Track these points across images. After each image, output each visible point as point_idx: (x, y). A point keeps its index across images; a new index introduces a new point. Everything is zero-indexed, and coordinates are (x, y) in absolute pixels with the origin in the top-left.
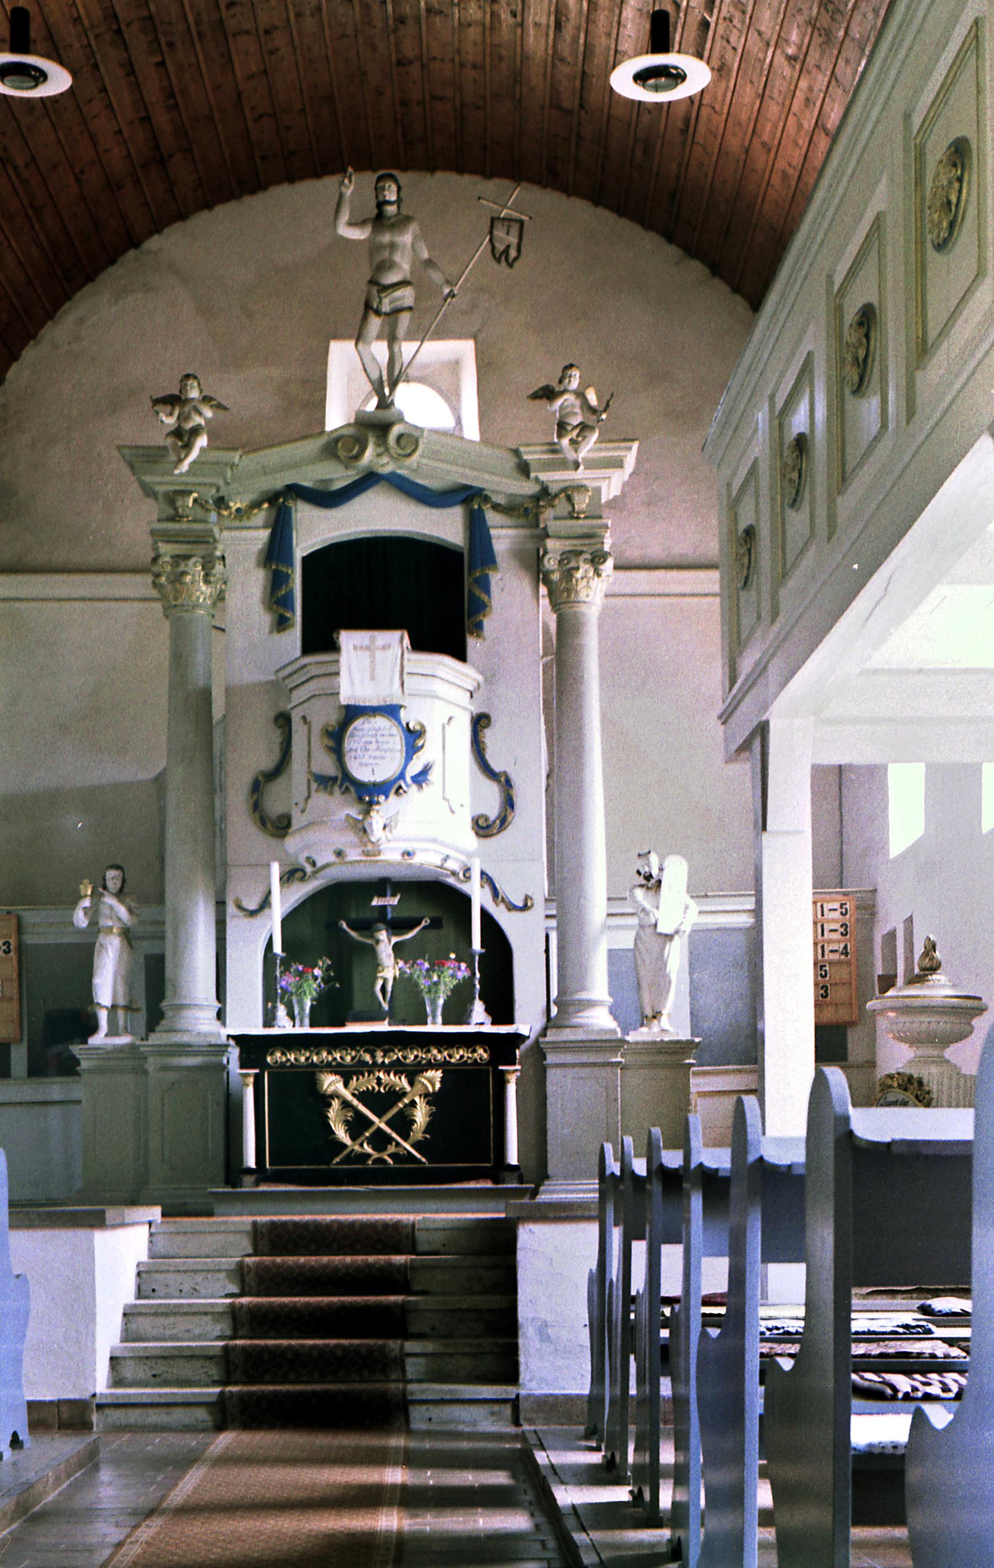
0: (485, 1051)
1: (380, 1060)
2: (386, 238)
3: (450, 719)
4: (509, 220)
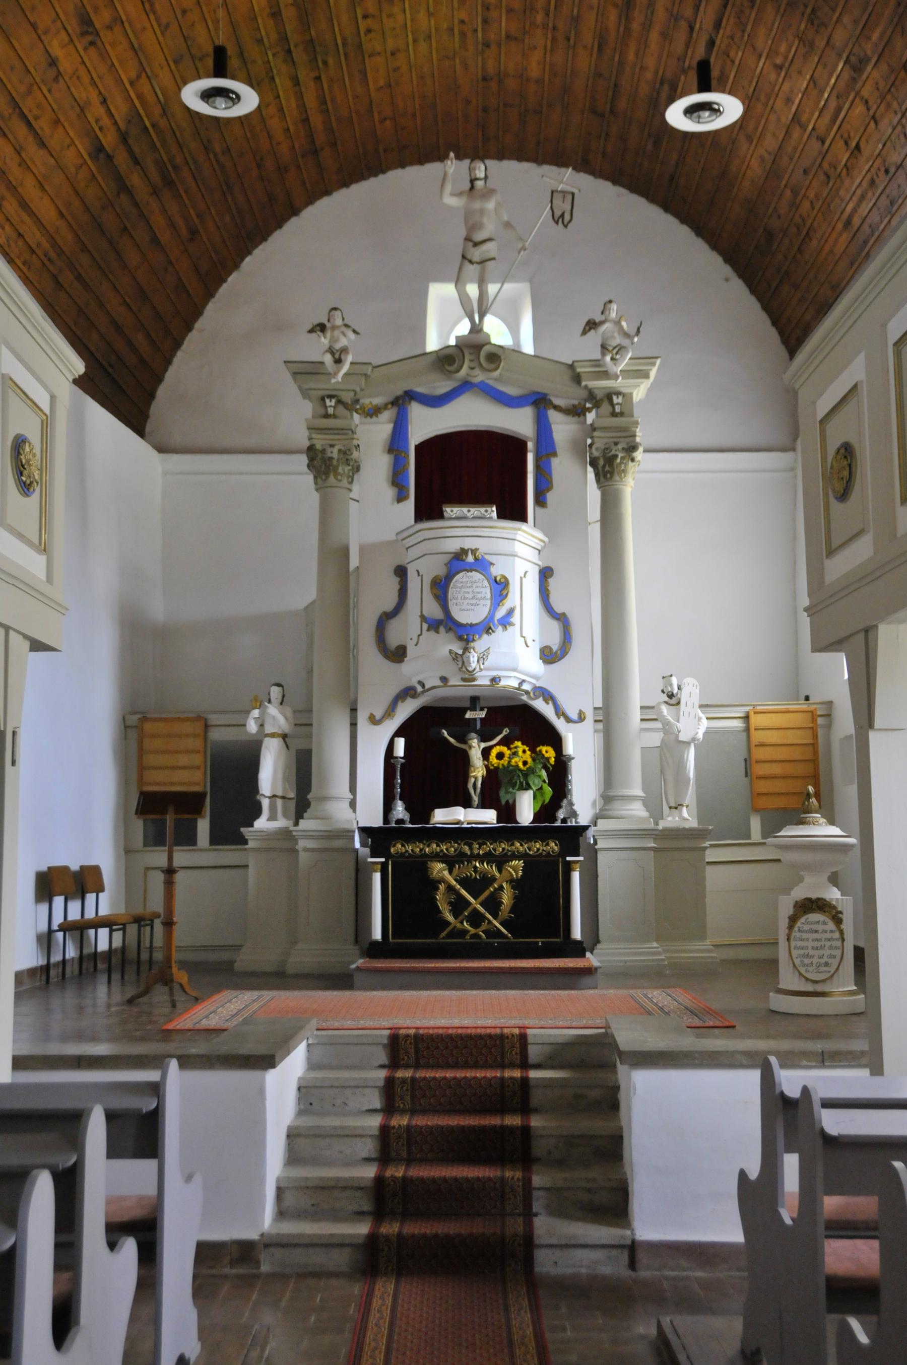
0: (556, 845)
1: (476, 852)
2: (477, 205)
3: (526, 573)
4: (564, 192)
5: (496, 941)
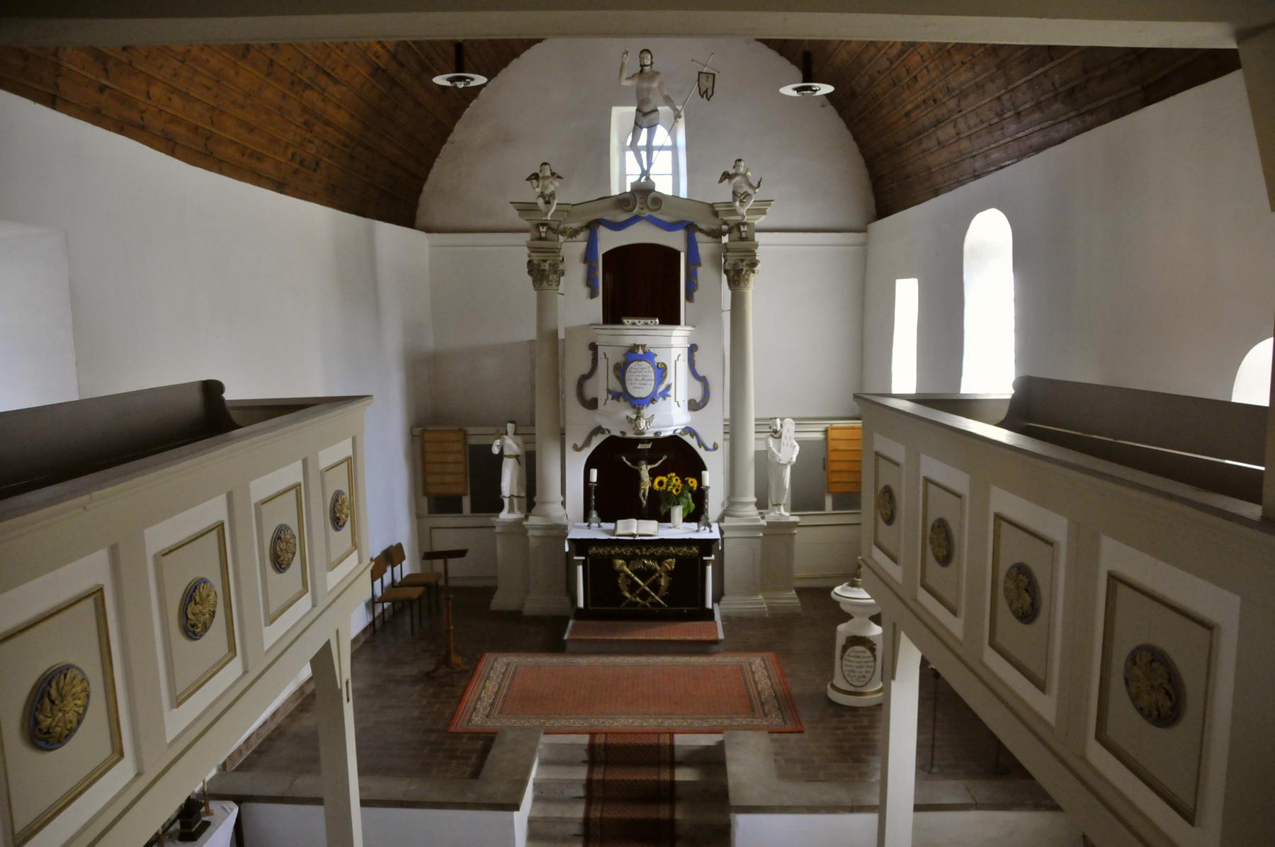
2: (645, 85)
5: (657, 609)
